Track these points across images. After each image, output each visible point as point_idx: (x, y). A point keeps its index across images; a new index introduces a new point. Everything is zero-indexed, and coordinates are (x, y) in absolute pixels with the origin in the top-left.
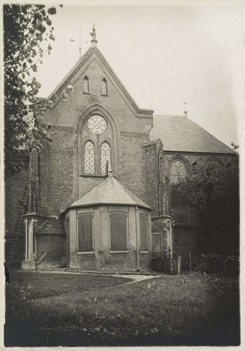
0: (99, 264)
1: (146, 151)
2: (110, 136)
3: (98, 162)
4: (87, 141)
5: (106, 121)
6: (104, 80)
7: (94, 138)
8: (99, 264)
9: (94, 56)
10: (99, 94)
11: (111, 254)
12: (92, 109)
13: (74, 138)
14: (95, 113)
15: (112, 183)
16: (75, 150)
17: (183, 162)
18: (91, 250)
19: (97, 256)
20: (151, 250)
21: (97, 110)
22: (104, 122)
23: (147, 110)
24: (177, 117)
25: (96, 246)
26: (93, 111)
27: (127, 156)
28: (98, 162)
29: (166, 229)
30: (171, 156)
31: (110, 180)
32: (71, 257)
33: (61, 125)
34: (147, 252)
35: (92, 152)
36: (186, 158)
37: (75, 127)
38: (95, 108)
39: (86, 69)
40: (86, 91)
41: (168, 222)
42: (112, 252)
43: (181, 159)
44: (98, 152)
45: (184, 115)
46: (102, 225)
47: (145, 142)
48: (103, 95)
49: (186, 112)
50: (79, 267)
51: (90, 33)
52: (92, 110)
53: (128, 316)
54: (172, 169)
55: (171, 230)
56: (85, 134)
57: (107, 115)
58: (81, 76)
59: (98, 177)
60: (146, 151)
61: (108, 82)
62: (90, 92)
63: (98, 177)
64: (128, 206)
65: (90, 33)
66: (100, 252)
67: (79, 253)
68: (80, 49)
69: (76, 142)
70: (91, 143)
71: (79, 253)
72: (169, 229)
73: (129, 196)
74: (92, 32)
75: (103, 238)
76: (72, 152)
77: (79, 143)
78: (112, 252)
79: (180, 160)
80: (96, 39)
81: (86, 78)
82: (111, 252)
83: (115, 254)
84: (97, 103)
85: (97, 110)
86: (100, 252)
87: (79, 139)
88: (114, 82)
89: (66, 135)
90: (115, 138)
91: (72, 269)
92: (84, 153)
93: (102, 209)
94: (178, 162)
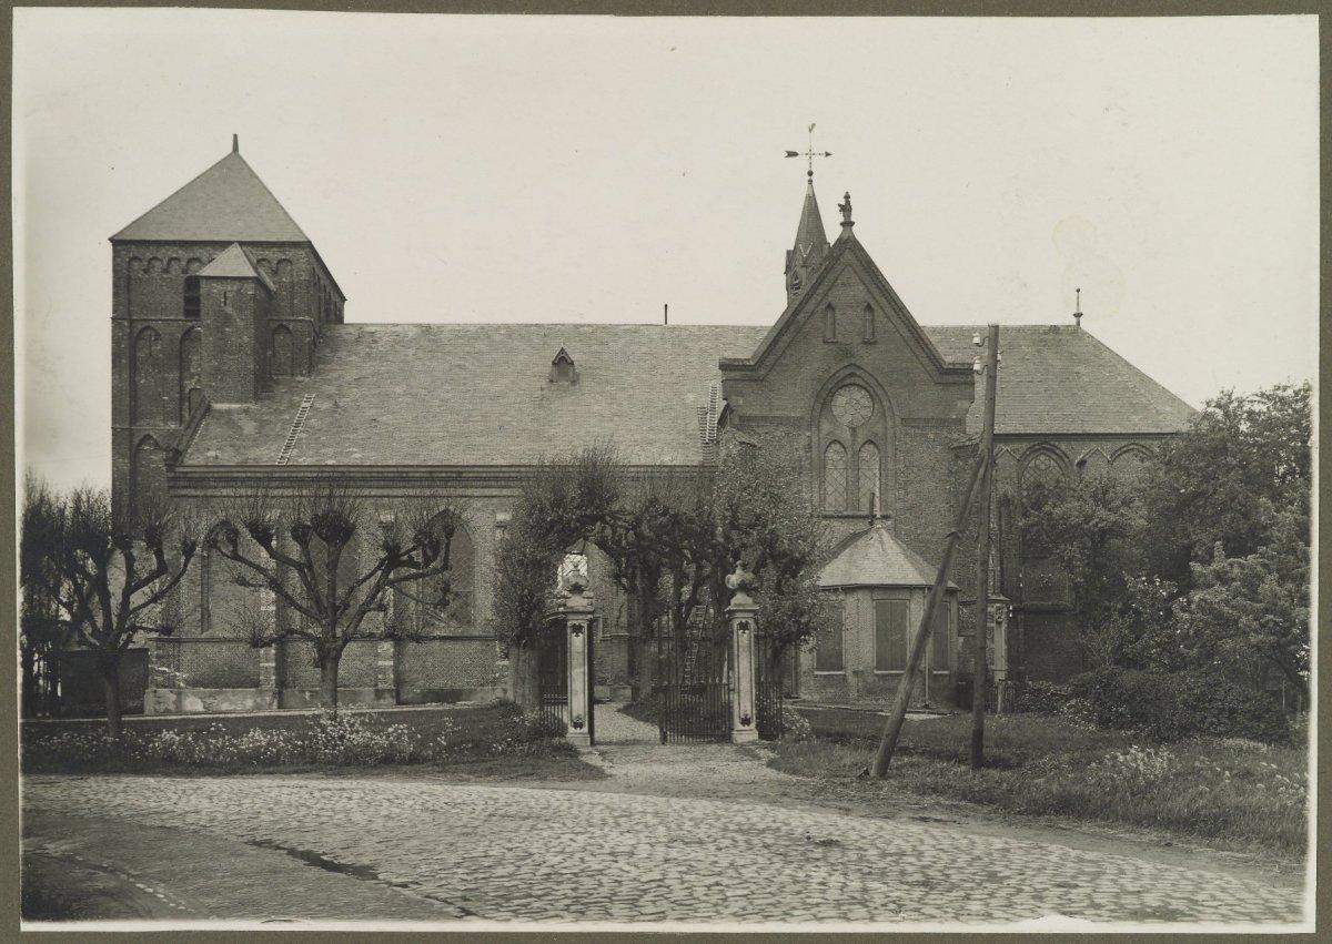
0: (853, 694)
1: (957, 457)
2: (879, 428)
3: (853, 487)
4: (830, 443)
5: (871, 396)
6: (869, 308)
7: (846, 436)
8: (853, 694)
9: (848, 256)
10: (858, 340)
11: (877, 675)
12: (842, 374)
13: (803, 441)
14: (848, 381)
15: (882, 543)
16: (806, 463)
17: (1054, 457)
18: (841, 668)
19: (852, 680)
20: (955, 665)
21: (852, 375)
22: (866, 402)
23: (963, 364)
24: (1055, 329)
25: (849, 660)
26: (844, 378)
27: (915, 469)
28: (853, 487)
29: (993, 625)
30: (1025, 446)
31: (876, 536)
32: (803, 679)
33: (778, 413)
34: (946, 672)
35: (841, 466)
36: (1063, 447)
37: (807, 417)
38: (847, 372)
39: (829, 289)
40: (829, 335)
41: (999, 609)
42: (879, 672)
43: (1048, 450)
44: (855, 465)
45: (1073, 321)
46: (859, 619)
47: (956, 436)
48: (865, 343)
49: (1078, 315)
50: (817, 697)
51: (840, 205)
52: (842, 376)
53: (211, 879)
54: (1028, 476)
55: (1004, 626)
56: (826, 427)
57: (873, 383)
58: (819, 305)
59: (853, 517)
60: (957, 457)
61: (878, 312)
62: (839, 338)
63: (853, 517)
64: (911, 588)
65: (840, 205)
66: (856, 673)
67: (816, 673)
68: (810, 174)
69: (809, 448)
70: (838, 446)
71: (816, 673)
72: (999, 623)
73: (912, 569)
74: (843, 203)
75: (860, 646)
76: (801, 468)
77: (814, 450)
78: (879, 672)
79: (1049, 453)
80: (853, 219)
81: (830, 307)
82: (875, 672)
83: (883, 675)
84: (853, 361)
85: (852, 375)
86: (856, 673)
87: (815, 439)
88: (889, 310)
89: (788, 434)
90: (890, 431)
91: (804, 701)
92: (825, 468)
93: (860, 595)
94: (1043, 458)
